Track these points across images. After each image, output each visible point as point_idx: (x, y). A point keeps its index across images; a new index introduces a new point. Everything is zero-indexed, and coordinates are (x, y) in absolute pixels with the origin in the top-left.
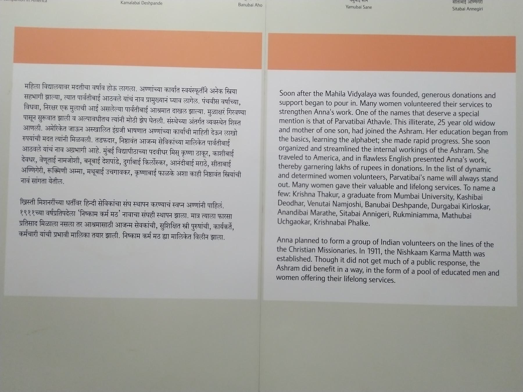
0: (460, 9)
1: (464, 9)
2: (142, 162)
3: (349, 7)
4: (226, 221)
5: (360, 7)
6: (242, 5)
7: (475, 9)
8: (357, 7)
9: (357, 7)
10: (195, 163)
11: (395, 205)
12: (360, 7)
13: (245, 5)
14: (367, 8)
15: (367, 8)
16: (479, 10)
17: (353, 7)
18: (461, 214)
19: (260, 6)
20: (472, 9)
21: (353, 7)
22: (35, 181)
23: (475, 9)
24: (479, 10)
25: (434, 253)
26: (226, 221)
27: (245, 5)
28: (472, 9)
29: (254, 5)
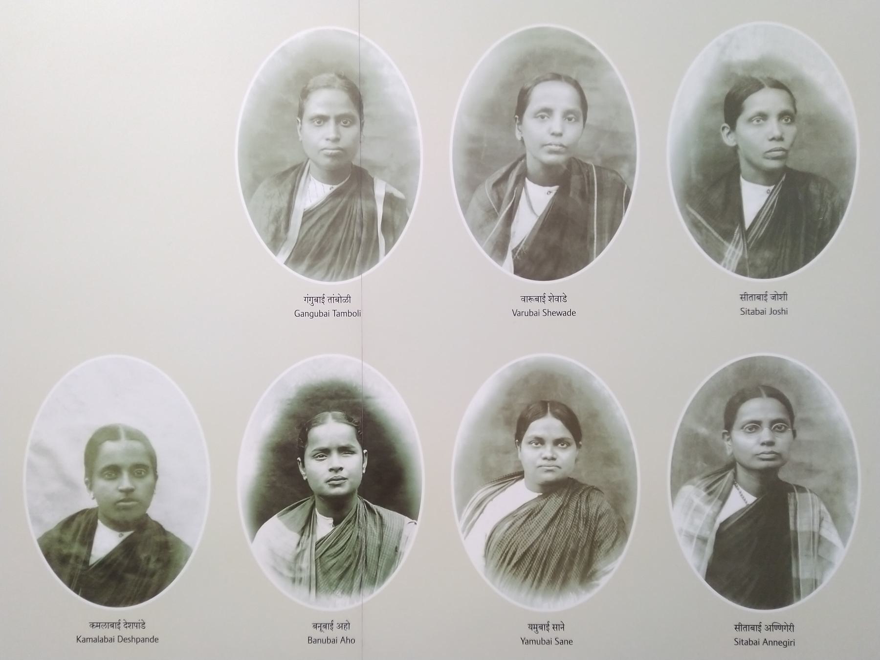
0: (755, 312)
1: (757, 643)
2: (122, 625)
3: (528, 642)
4: (745, 635)
5: (549, 642)
6: (316, 641)
7: (779, 643)
8: (542, 642)
9: (542, 642)
10: (551, 627)
11: (120, 639)
12: (549, 642)
13: (322, 641)
14: (562, 642)
15: (562, 642)
16: (787, 644)
17: (536, 642)
18: (325, 638)
19: (351, 641)
20: (773, 643)
21: (536, 642)
22: (137, 640)
23: (779, 643)
24: (787, 644)
25: (81, 639)
26: (745, 635)
27: (322, 641)
28: (773, 643)
29: (761, 643)
